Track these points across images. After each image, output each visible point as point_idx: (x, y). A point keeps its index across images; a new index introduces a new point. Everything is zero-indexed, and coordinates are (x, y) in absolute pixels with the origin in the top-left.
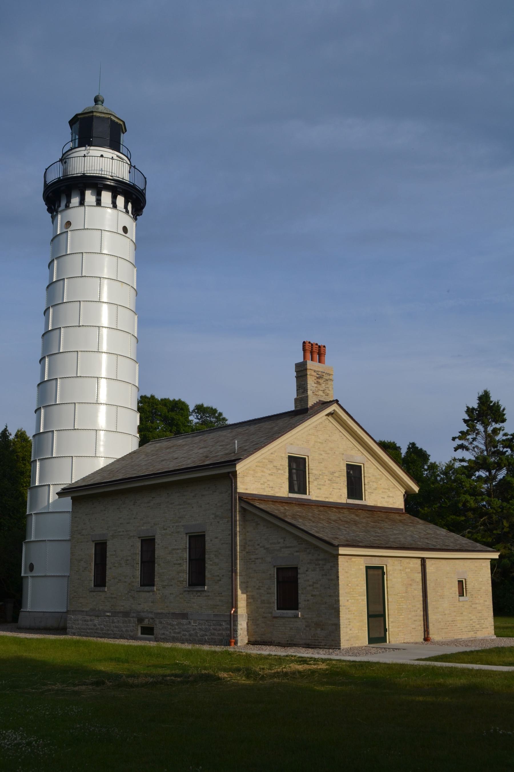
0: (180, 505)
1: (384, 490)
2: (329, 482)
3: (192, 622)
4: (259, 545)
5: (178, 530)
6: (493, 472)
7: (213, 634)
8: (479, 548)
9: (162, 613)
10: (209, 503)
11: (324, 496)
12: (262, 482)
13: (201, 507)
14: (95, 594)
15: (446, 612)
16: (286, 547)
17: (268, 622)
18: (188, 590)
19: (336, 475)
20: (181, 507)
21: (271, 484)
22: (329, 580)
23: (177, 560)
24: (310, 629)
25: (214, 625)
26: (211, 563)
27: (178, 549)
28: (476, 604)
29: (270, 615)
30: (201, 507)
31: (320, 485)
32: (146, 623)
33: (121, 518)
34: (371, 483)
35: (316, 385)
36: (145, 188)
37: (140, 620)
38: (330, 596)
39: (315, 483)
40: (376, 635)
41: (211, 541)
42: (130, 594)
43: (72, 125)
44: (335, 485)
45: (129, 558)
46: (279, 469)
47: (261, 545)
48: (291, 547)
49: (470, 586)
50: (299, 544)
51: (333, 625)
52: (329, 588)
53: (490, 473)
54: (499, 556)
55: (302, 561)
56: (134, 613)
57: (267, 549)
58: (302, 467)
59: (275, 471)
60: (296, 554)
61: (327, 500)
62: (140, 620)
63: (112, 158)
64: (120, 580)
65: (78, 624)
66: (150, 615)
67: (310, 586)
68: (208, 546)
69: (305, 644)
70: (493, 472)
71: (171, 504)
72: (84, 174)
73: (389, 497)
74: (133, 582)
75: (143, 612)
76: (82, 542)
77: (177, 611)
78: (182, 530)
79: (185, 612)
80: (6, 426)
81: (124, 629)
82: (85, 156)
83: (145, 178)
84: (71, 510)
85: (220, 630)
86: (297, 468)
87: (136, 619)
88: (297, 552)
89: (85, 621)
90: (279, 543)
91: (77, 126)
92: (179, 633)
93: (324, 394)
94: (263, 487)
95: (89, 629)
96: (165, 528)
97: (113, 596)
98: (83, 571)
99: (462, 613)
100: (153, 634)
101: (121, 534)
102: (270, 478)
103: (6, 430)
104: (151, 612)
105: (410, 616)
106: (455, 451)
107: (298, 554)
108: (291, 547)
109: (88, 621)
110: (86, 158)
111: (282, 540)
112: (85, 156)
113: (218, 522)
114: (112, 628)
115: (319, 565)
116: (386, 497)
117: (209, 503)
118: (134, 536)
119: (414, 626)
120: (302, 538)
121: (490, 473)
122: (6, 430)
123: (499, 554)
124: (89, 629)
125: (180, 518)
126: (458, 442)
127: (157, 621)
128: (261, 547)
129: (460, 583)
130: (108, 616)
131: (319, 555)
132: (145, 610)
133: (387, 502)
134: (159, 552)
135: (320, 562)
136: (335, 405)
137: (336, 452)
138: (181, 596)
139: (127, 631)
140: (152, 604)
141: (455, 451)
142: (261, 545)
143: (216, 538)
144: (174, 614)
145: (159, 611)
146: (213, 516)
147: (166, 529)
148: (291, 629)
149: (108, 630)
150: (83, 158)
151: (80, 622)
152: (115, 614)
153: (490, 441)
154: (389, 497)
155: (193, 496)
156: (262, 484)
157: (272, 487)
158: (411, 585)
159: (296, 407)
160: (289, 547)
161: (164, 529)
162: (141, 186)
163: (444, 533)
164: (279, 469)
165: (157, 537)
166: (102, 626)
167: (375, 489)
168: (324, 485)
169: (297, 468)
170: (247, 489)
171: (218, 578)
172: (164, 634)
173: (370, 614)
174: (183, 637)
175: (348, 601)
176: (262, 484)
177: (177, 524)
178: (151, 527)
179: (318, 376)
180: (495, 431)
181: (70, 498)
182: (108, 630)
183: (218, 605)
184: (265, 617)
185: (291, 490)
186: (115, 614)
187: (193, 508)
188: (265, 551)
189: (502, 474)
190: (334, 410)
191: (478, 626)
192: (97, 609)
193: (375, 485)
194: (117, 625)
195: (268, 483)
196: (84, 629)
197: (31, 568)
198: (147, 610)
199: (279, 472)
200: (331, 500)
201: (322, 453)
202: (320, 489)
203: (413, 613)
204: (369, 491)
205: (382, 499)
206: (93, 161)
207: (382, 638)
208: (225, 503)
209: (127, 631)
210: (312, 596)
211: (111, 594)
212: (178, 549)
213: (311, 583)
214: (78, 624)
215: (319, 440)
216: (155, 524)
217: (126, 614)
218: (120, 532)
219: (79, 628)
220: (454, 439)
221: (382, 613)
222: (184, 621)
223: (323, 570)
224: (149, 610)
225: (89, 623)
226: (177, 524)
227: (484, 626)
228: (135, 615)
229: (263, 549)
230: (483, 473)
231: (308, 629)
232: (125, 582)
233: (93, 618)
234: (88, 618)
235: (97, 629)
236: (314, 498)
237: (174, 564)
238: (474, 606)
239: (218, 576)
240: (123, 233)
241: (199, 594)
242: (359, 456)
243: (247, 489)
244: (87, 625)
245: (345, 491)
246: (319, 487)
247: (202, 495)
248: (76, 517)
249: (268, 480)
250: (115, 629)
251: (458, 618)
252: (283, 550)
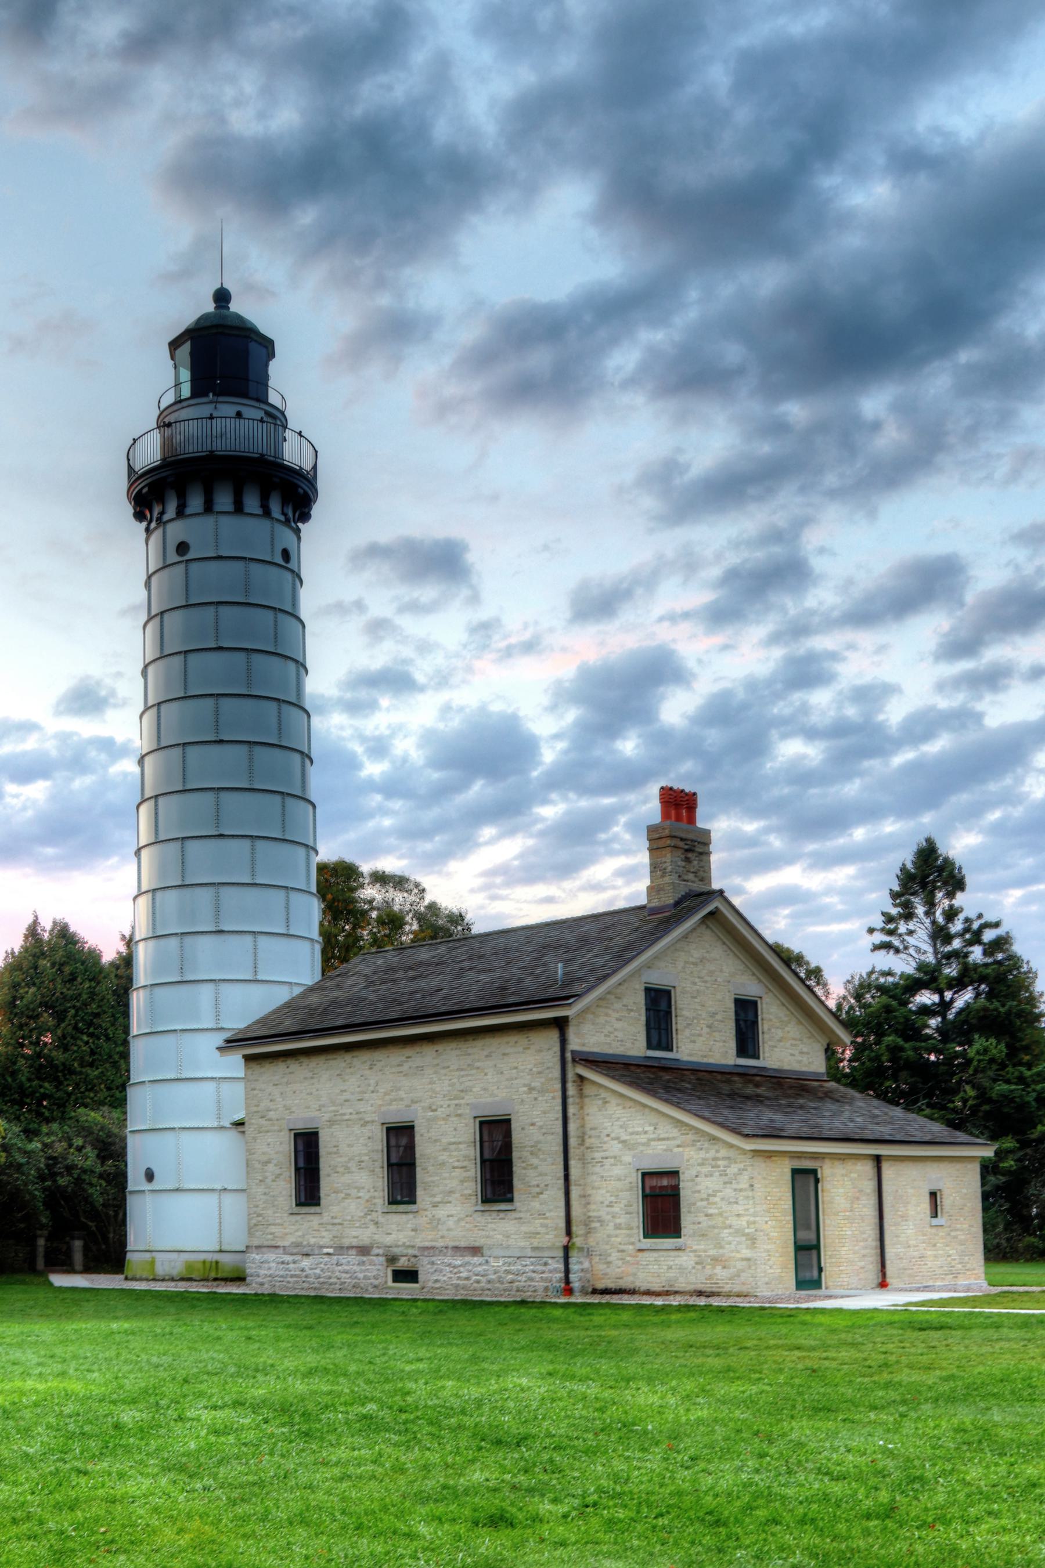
0: (462, 1070)
1: (794, 1042)
2: (708, 1030)
3: (491, 1260)
4: (608, 1135)
5: (459, 1112)
6: (948, 995)
7: (531, 1279)
8: (959, 1140)
9: (433, 1248)
10: (516, 1068)
11: (701, 1053)
12: (606, 1032)
13: (502, 1073)
14: (298, 1218)
15: (911, 1243)
16: (659, 1140)
17: (628, 1258)
18: (483, 1209)
19: (718, 1017)
20: (462, 1073)
21: (620, 1035)
22: (735, 1190)
23: (458, 1161)
24: (704, 1268)
25: (532, 1264)
26: (524, 1165)
27: (460, 1143)
28: (957, 1230)
29: (631, 1247)
30: (502, 1073)
31: (693, 1035)
32: (403, 1263)
33: (345, 1091)
34: (773, 1030)
35: (683, 864)
36: (315, 467)
37: (392, 1259)
38: (738, 1215)
39: (687, 1032)
40: (807, 1275)
41: (523, 1129)
42: (369, 1217)
43: (175, 349)
44: (716, 1034)
45: (366, 1158)
46: (632, 1010)
47: (613, 1135)
48: (668, 1139)
49: (926, 1205)
50: (683, 1134)
51: (743, 1259)
52: (737, 1203)
53: (942, 997)
54: (996, 1153)
55: (688, 1161)
56: (378, 1247)
57: (624, 1142)
58: (663, 1006)
59: (625, 1014)
60: (676, 1150)
61: (705, 1060)
62: (392, 1259)
63: (262, 421)
64: (349, 1195)
65: (269, 1269)
66: (411, 1252)
67: (702, 1200)
68: (517, 1137)
69: (695, 1291)
70: (948, 995)
71: (444, 1068)
72: (212, 452)
73: (801, 1053)
74: (375, 1198)
75: (397, 1246)
76: (268, 1131)
77: (463, 1244)
78: (468, 1111)
79: (477, 1244)
80: (36, 917)
81: (361, 1276)
82: (211, 418)
83: (316, 452)
84: (243, 1075)
85: (543, 1272)
86: (659, 1006)
87: (382, 1259)
88: (678, 1146)
89: (283, 1263)
90: (646, 1132)
91: (186, 348)
92: (467, 1279)
93: (696, 879)
94: (608, 1040)
95: (292, 1276)
96: (434, 1107)
97: (336, 1221)
98: (273, 1181)
99: (935, 1245)
100: (416, 1281)
101: (347, 1117)
102: (618, 1025)
103: (36, 922)
104: (413, 1247)
105: (856, 1248)
106: (873, 950)
107: (681, 1149)
108: (668, 1139)
109: (288, 1264)
110: (214, 421)
111: (652, 1128)
112: (211, 418)
113: (536, 1099)
114: (337, 1274)
115: (719, 1167)
116: (796, 1053)
117: (516, 1068)
118: (373, 1121)
119: (862, 1264)
120: (687, 1125)
121: (942, 997)
122: (36, 922)
123: (994, 1148)
124: (292, 1276)
125: (462, 1091)
126: (879, 938)
127: (425, 1261)
128: (613, 1139)
129: (933, 1195)
130: (328, 1254)
131: (717, 1151)
132: (400, 1243)
133: (799, 1062)
134: (423, 1148)
135: (720, 1163)
136: (719, 898)
137: (719, 979)
138: (468, 1219)
139: (365, 1278)
140: (413, 1233)
141: (873, 950)
142: (613, 1135)
143: (533, 1124)
144: (456, 1248)
145: (427, 1244)
146: (525, 1089)
147: (436, 1110)
148: (670, 1268)
149: (330, 1278)
150: (209, 421)
151: (273, 1265)
152: (341, 1249)
153: (940, 935)
154: (801, 1053)
155: (487, 1056)
156: (606, 1036)
157: (622, 1041)
158: (858, 1199)
159: (649, 901)
160: (664, 1139)
161: (433, 1111)
162: (307, 466)
163: (901, 1115)
164: (632, 1010)
165: (416, 1124)
166: (318, 1271)
167: (780, 1041)
168: (700, 1035)
169: (659, 1006)
170: (584, 1045)
171: (538, 1190)
172: (437, 1281)
173: (799, 1243)
174: (475, 1285)
175: (766, 1222)
176: (606, 1036)
177: (457, 1102)
178: (407, 1106)
179: (686, 847)
180: (951, 914)
181: (241, 1056)
182: (330, 1278)
183: (538, 1233)
184: (623, 1251)
185: (650, 1046)
186: (341, 1249)
187: (486, 1074)
188: (620, 1145)
189: (964, 998)
190: (716, 907)
191: (960, 1266)
192: (305, 1243)
193: (780, 1033)
194: (347, 1268)
195: (616, 1034)
196: (282, 1276)
197: (150, 1176)
198: (404, 1243)
199: (632, 1014)
200: (711, 1061)
201: (697, 980)
202: (694, 1042)
203: (862, 1244)
204: (771, 1043)
205: (790, 1058)
206: (224, 424)
207: (815, 1281)
208: (548, 1068)
209: (365, 1278)
210: (706, 1215)
211: (332, 1218)
212: (460, 1143)
213: (705, 1196)
214: (269, 1269)
215: (691, 959)
216: (413, 1102)
217: (364, 1250)
218: (344, 1114)
219: (270, 1276)
220: (871, 931)
221: (815, 1243)
222: (476, 1260)
223: (726, 1175)
224: (408, 1244)
225: (291, 1266)
226: (457, 1102)
227: (969, 1266)
228: (381, 1251)
229: (616, 1142)
230: (926, 998)
231: (699, 1267)
232: (359, 1198)
233: (298, 1258)
234: (288, 1258)
235: (306, 1277)
236: (685, 1058)
237: (454, 1168)
238: (953, 1234)
239: (538, 1186)
240: (282, 563)
241: (502, 1215)
242: (751, 987)
243: (584, 1045)
244: (287, 1269)
245: (732, 1045)
246: (693, 1038)
247: (504, 1054)
248: (254, 1089)
249: (616, 1030)
250: (344, 1275)
251: (929, 1253)
252: (652, 1143)
